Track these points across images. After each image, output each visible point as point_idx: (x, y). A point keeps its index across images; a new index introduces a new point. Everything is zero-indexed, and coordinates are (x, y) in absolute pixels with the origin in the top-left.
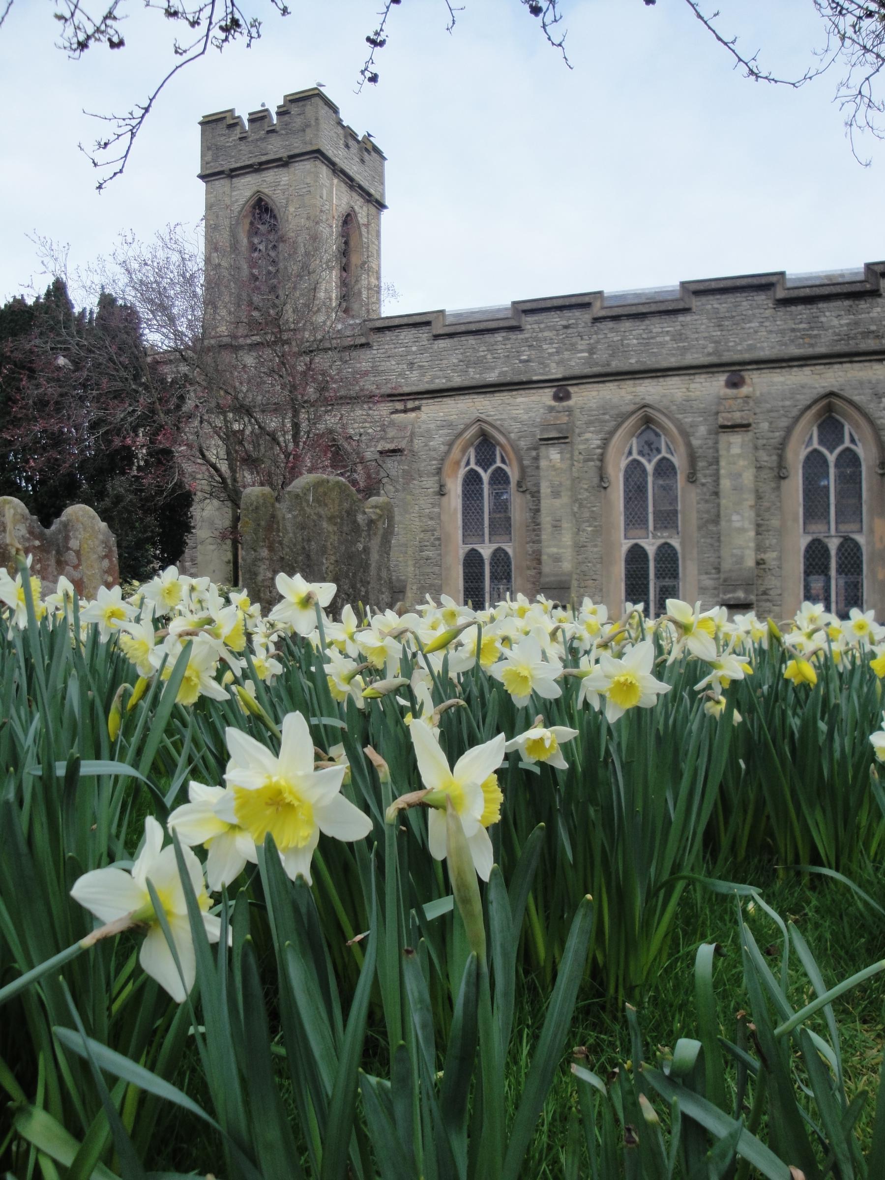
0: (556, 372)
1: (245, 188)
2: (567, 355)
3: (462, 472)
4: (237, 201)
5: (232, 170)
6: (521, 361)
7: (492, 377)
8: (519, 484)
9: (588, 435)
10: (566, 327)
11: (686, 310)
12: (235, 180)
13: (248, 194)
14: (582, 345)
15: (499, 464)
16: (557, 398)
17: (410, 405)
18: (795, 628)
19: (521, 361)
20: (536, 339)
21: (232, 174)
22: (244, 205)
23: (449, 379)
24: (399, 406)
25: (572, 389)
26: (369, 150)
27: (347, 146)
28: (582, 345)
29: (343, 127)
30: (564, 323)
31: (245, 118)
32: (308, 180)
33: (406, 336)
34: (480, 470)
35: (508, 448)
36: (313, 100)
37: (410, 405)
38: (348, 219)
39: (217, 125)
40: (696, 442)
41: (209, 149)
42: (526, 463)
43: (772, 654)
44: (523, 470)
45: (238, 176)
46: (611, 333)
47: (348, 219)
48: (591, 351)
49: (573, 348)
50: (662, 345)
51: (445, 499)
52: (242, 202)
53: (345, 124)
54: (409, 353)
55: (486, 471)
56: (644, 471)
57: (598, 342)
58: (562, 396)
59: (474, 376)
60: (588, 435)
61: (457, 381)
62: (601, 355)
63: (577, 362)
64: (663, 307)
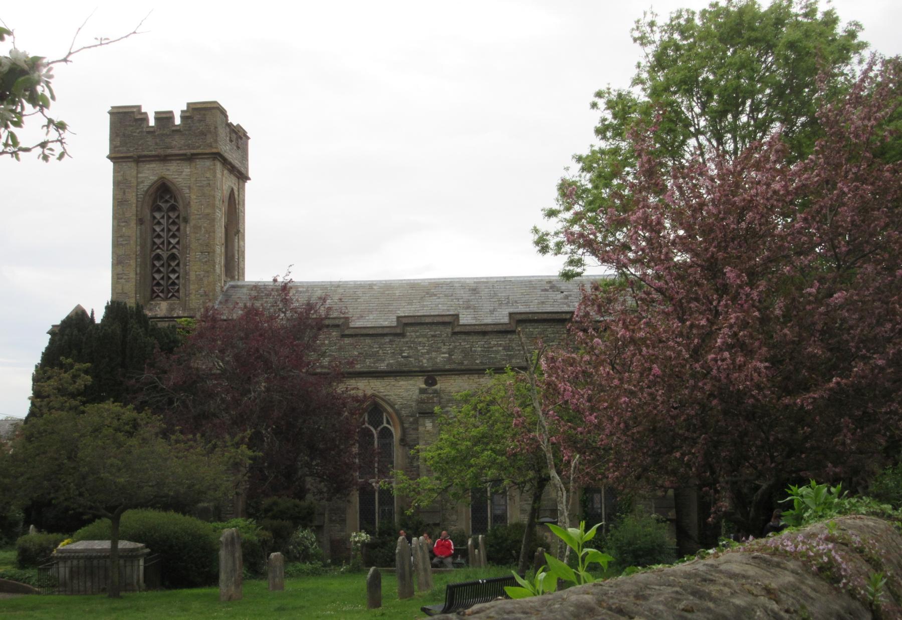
2: (434, 354)
4: (142, 182)
5: (139, 157)
6: (403, 357)
7: (383, 366)
10: (433, 336)
11: (513, 332)
12: (140, 164)
13: (154, 178)
14: (444, 349)
15: (385, 424)
16: (426, 383)
18: (556, 206)
19: (403, 357)
20: (414, 342)
21: (139, 160)
22: (150, 187)
28: (444, 349)
30: (432, 333)
32: (208, 175)
35: (394, 415)
36: (213, 111)
39: (125, 122)
41: (117, 135)
42: (406, 425)
43: (253, 304)
44: (404, 431)
45: (144, 161)
46: (464, 343)
48: (451, 353)
49: (438, 350)
50: (497, 352)
52: (147, 184)
55: (376, 429)
57: (455, 347)
58: (431, 381)
63: (441, 358)
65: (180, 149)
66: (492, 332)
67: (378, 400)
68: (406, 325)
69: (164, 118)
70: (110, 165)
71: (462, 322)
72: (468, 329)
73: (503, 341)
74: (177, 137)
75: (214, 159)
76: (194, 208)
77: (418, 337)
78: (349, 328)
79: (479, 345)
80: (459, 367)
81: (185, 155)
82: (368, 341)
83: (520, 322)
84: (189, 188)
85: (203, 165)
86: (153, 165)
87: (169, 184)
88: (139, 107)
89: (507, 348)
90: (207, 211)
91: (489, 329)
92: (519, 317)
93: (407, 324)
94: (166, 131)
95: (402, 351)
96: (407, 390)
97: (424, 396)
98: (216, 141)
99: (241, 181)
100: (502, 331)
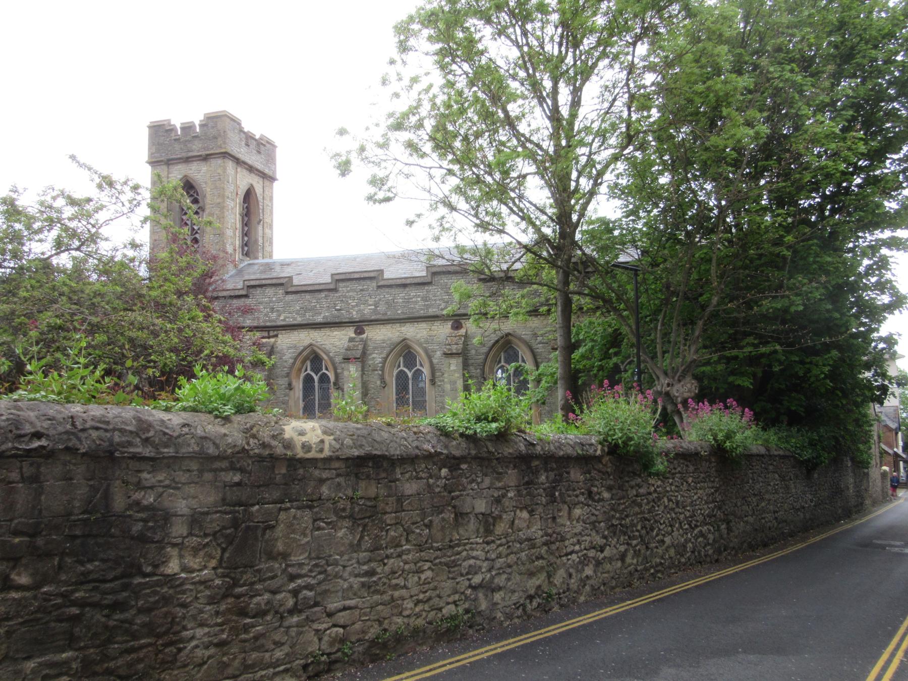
0: (355, 315)
1: (176, 175)
3: (303, 375)
5: (169, 160)
7: (319, 319)
8: (335, 384)
9: (374, 355)
10: (361, 290)
12: (171, 167)
14: (371, 302)
15: (324, 371)
16: (355, 332)
17: (272, 333)
20: (345, 297)
21: (169, 163)
23: (295, 319)
24: (266, 334)
25: (463, 321)
26: (264, 146)
27: (247, 145)
29: (244, 133)
31: (178, 126)
32: (219, 171)
33: (270, 291)
34: (313, 374)
37: (272, 333)
38: (249, 196)
40: (435, 361)
46: (387, 295)
47: (249, 196)
48: (376, 305)
49: (366, 303)
50: (417, 302)
51: (292, 392)
53: (246, 130)
54: (271, 301)
56: (407, 376)
58: (360, 331)
59: (309, 317)
60: (374, 355)
61: (299, 320)
62: (382, 308)
63: (367, 311)
64: (416, 281)
65: (199, 151)
66: (411, 284)
67: (315, 348)
68: (338, 281)
69: (188, 128)
70: (149, 168)
71: (385, 277)
72: (391, 282)
73: (421, 292)
74: (196, 142)
75: (224, 157)
76: (208, 200)
77: (348, 292)
78: (292, 286)
79: (400, 296)
80: (383, 318)
81: (200, 156)
82: (308, 296)
83: (434, 274)
84: (206, 183)
85: (216, 163)
86: (180, 166)
87: (194, 184)
88: (169, 120)
89: (425, 299)
90: (218, 201)
91: (408, 281)
92: (434, 270)
93: (342, 280)
94: (188, 138)
95: (335, 305)
96: (340, 340)
97: (351, 344)
98: (225, 143)
99: (267, 183)
100: (421, 284)
